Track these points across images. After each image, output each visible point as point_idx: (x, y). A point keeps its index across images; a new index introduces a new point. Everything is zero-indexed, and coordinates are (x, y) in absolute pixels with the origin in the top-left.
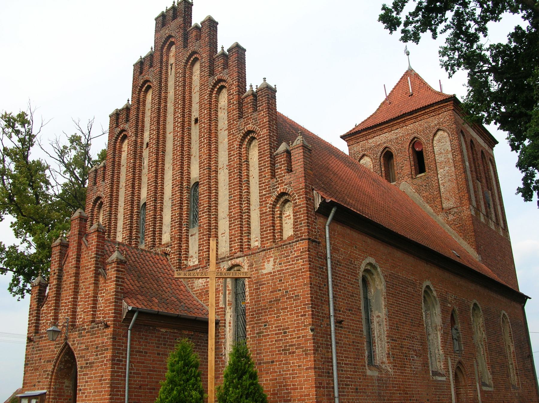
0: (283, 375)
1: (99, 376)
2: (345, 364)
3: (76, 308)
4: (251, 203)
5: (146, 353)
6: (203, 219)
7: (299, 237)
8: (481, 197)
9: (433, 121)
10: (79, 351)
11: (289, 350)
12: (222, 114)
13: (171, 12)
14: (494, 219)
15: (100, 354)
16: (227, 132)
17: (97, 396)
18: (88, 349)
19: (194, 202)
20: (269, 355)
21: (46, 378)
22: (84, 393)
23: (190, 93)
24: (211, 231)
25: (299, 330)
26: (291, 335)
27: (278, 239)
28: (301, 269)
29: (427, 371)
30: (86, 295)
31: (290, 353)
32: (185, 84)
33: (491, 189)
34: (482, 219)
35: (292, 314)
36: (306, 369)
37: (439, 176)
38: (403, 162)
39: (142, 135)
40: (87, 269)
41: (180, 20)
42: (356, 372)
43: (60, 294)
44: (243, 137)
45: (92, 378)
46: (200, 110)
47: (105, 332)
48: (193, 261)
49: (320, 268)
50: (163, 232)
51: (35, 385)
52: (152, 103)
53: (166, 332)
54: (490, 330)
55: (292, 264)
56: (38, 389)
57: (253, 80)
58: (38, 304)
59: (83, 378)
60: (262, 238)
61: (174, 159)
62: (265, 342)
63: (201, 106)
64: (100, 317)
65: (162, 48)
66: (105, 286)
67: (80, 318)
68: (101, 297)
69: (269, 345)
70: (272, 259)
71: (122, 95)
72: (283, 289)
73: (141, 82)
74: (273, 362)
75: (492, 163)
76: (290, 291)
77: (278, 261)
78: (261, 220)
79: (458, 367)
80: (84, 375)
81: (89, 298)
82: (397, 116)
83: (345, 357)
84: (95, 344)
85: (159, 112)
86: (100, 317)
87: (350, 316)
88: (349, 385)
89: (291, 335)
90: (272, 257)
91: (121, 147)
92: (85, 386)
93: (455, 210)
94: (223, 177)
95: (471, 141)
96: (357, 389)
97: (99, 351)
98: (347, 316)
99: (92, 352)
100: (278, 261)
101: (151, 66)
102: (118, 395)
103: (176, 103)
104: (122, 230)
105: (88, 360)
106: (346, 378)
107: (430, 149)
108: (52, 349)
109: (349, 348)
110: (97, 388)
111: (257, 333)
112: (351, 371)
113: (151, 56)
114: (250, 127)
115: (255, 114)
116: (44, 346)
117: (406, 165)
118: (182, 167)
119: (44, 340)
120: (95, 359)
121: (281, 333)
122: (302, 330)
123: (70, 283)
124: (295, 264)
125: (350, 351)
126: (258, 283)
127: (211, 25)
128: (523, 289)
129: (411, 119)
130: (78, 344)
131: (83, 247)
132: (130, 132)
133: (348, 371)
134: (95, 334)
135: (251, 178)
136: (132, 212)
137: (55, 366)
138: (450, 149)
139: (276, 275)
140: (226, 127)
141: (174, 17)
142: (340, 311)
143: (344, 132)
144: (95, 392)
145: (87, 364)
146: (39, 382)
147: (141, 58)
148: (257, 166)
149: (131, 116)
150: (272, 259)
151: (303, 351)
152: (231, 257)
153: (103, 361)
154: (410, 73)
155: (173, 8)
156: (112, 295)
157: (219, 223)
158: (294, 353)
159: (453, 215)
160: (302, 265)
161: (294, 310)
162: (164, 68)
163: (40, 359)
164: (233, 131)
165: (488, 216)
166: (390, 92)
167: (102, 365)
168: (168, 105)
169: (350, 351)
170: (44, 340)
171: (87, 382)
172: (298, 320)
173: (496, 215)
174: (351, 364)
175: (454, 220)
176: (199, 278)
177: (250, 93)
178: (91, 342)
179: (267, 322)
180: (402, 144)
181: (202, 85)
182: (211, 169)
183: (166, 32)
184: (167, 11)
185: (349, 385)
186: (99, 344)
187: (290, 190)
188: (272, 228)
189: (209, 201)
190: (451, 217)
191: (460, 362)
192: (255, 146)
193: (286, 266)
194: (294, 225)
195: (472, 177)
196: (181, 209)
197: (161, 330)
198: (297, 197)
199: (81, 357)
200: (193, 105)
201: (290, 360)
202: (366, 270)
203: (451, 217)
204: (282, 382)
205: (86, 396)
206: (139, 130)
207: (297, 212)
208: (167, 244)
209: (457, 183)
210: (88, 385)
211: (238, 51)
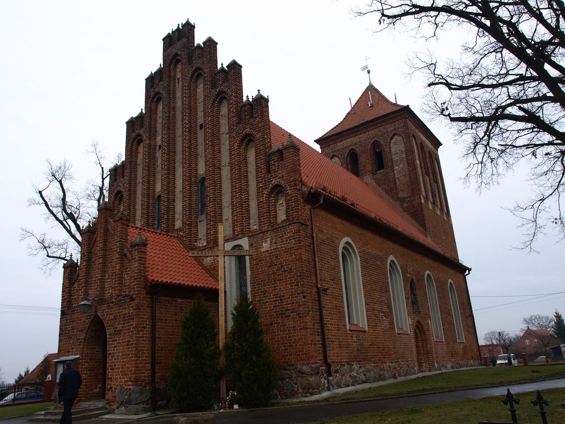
0: (280, 335)
1: (126, 342)
2: (331, 324)
3: (104, 285)
4: (250, 193)
5: (166, 320)
6: (210, 208)
7: (291, 221)
8: (429, 188)
9: (391, 127)
10: (108, 320)
11: (285, 314)
12: (224, 121)
13: (177, 33)
14: (439, 206)
15: (127, 323)
16: (228, 136)
17: (124, 358)
18: (116, 319)
20: (268, 319)
21: (79, 345)
22: (114, 356)
23: (196, 103)
24: (217, 218)
25: (293, 297)
26: (286, 302)
27: (273, 223)
28: (293, 248)
29: (393, 329)
30: (113, 273)
31: (286, 317)
32: (191, 96)
33: (437, 182)
34: (430, 207)
35: (287, 284)
36: (300, 329)
37: (395, 172)
39: (155, 139)
40: (112, 252)
41: (184, 40)
42: (339, 331)
43: (89, 273)
44: (242, 139)
45: (120, 343)
46: (205, 118)
47: (131, 304)
48: (202, 243)
49: (309, 246)
50: (176, 220)
51: (69, 352)
52: (163, 112)
53: (182, 302)
54: (440, 295)
55: (286, 243)
56: (72, 355)
57: (249, 92)
58: (70, 282)
60: (259, 222)
61: (183, 159)
62: (265, 308)
63: (205, 114)
64: (126, 292)
65: (170, 64)
66: (129, 265)
67: (108, 293)
68: (127, 274)
69: (269, 310)
70: (269, 240)
71: (136, 105)
72: (279, 264)
73: (153, 94)
74: (271, 324)
76: (285, 265)
77: (274, 241)
78: (258, 207)
79: (417, 326)
80: (113, 341)
81: (116, 275)
82: (360, 123)
83: (330, 319)
84: (123, 315)
85: (169, 120)
86: (126, 292)
87: (333, 285)
88: (334, 342)
89: (286, 302)
90: (269, 238)
91: (137, 149)
92: (114, 350)
93: (409, 199)
94: (226, 173)
95: (421, 143)
96: (340, 345)
97: (125, 320)
98: (331, 285)
99: (120, 321)
100: (274, 241)
101: (161, 80)
102: (143, 357)
103: (183, 112)
104: (140, 218)
105: (117, 328)
106: (331, 335)
107: (387, 150)
108: (83, 321)
109: (333, 311)
110: (125, 352)
111: (258, 301)
113: (160, 72)
114: (247, 131)
115: (252, 120)
116: (76, 318)
117: (368, 164)
118: (190, 165)
119: (77, 313)
120: (122, 327)
121: (278, 300)
122: (296, 297)
123: (99, 264)
124: (289, 243)
125: (334, 314)
126: (257, 259)
127: (211, 44)
128: (464, 259)
129: (372, 126)
131: (462, 124)
133: (332, 330)
134: (122, 306)
135: (249, 173)
136: (148, 203)
137: (86, 334)
138: (404, 150)
139: (272, 253)
140: (227, 131)
141: (179, 38)
142: (325, 281)
143: (317, 137)
144: (123, 355)
145: (115, 331)
146: (73, 349)
147: (152, 74)
148: (254, 163)
149: (145, 123)
150: (269, 240)
151: (297, 315)
152: (235, 238)
153: (130, 329)
154: (371, 88)
156: (136, 273)
157: (223, 211)
158: (289, 316)
159: (407, 203)
160: (294, 244)
161: (288, 281)
162: (172, 82)
163: (73, 329)
164: (234, 135)
165: (434, 204)
167: (128, 332)
168: (177, 113)
169: (334, 314)
170: (77, 313)
171: (116, 347)
172: (292, 289)
173: (441, 203)
175: (408, 207)
176: (207, 257)
178: (118, 313)
179: (266, 291)
180: (365, 146)
181: (205, 96)
182: (214, 167)
183: (172, 51)
184: (173, 32)
185: (334, 342)
186: (126, 314)
187: (282, 183)
188: (268, 213)
189: (214, 193)
190: (405, 205)
191: (418, 322)
192: (252, 147)
193: (280, 245)
194: (286, 211)
195: (422, 173)
196: (190, 199)
197: (179, 300)
198: (288, 188)
199: (110, 326)
200: (198, 113)
201: (286, 322)
202: (344, 248)
203: (405, 205)
204: (280, 341)
205: (115, 359)
206: (153, 135)
207: (289, 200)
208: (180, 229)
209: (410, 178)
210: (117, 350)
211: (235, 67)
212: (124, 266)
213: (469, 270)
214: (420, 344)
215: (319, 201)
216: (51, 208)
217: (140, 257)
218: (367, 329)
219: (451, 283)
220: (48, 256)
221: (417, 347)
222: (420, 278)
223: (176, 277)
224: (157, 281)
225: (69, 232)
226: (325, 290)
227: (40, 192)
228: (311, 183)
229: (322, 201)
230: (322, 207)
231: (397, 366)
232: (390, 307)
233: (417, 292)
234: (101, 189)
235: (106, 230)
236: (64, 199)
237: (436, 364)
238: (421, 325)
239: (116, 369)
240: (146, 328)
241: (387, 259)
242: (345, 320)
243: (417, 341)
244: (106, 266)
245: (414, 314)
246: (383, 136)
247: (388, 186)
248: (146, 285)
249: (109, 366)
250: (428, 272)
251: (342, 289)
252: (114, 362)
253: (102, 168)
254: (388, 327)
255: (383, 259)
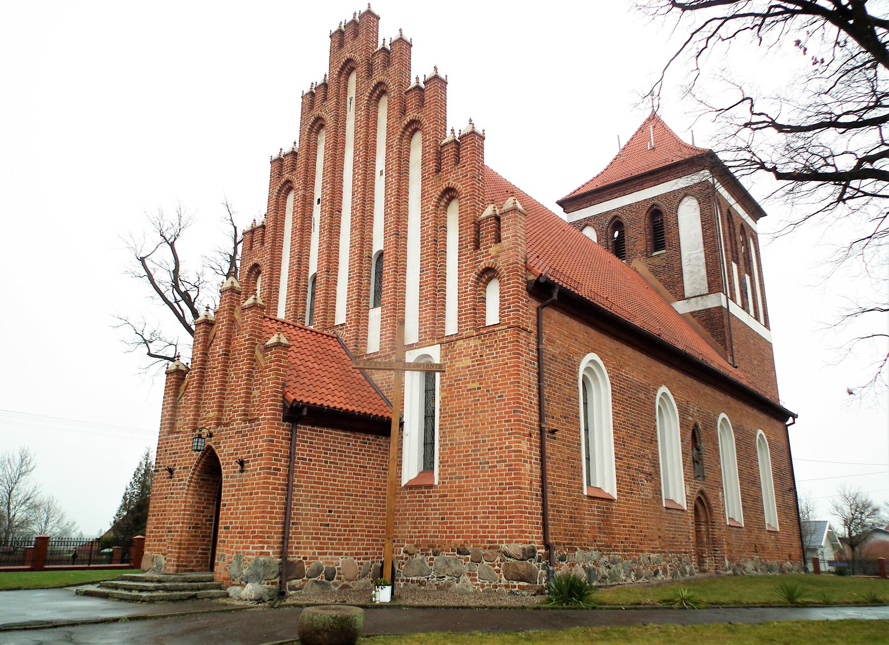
2: (558, 485)
6: (386, 298)
19: (378, 276)
22: (230, 509)
33: (751, 274)
38: (637, 235)
42: (571, 495)
54: (741, 453)
57: (456, 123)
59: (229, 491)
71: (287, 135)
75: (753, 240)
79: (699, 498)
87: (565, 425)
95: (729, 211)
106: (558, 502)
107: (672, 220)
112: (564, 494)
125: (564, 469)
128: (786, 401)
130: (225, 447)
132: (298, 184)
142: (553, 418)
151: (506, 466)
155: (353, 21)
156: (271, 388)
166: (625, 143)
169: (564, 469)
174: (564, 486)
177: (415, 88)
180: (636, 212)
182: (398, 234)
188: (474, 309)
191: (701, 492)
199: (227, 464)
202: (588, 369)
205: (232, 514)
206: (309, 183)
211: (437, 82)
212: (253, 377)
213: (795, 416)
214: (703, 528)
215: (551, 295)
216: (157, 283)
217: (277, 365)
218: (616, 497)
219: (761, 435)
220: (149, 354)
221: (698, 531)
222: (711, 425)
223: (329, 397)
224: (301, 401)
225: (182, 319)
226: (553, 432)
227: (142, 260)
228: (542, 268)
229: (555, 297)
230: (555, 305)
231: (661, 558)
232: (655, 465)
233: (703, 445)
234: (233, 259)
235: (232, 322)
236: (176, 272)
237: (727, 562)
238: (706, 498)
239: (233, 528)
240: (279, 470)
241: (656, 390)
242: (581, 480)
243: (697, 523)
244: (227, 375)
245: (695, 478)
246: (673, 197)
247: (669, 277)
248: (284, 406)
249: (222, 523)
250: (723, 415)
251: (579, 433)
252: (230, 518)
253: (235, 228)
254: (651, 496)
255: (650, 392)
